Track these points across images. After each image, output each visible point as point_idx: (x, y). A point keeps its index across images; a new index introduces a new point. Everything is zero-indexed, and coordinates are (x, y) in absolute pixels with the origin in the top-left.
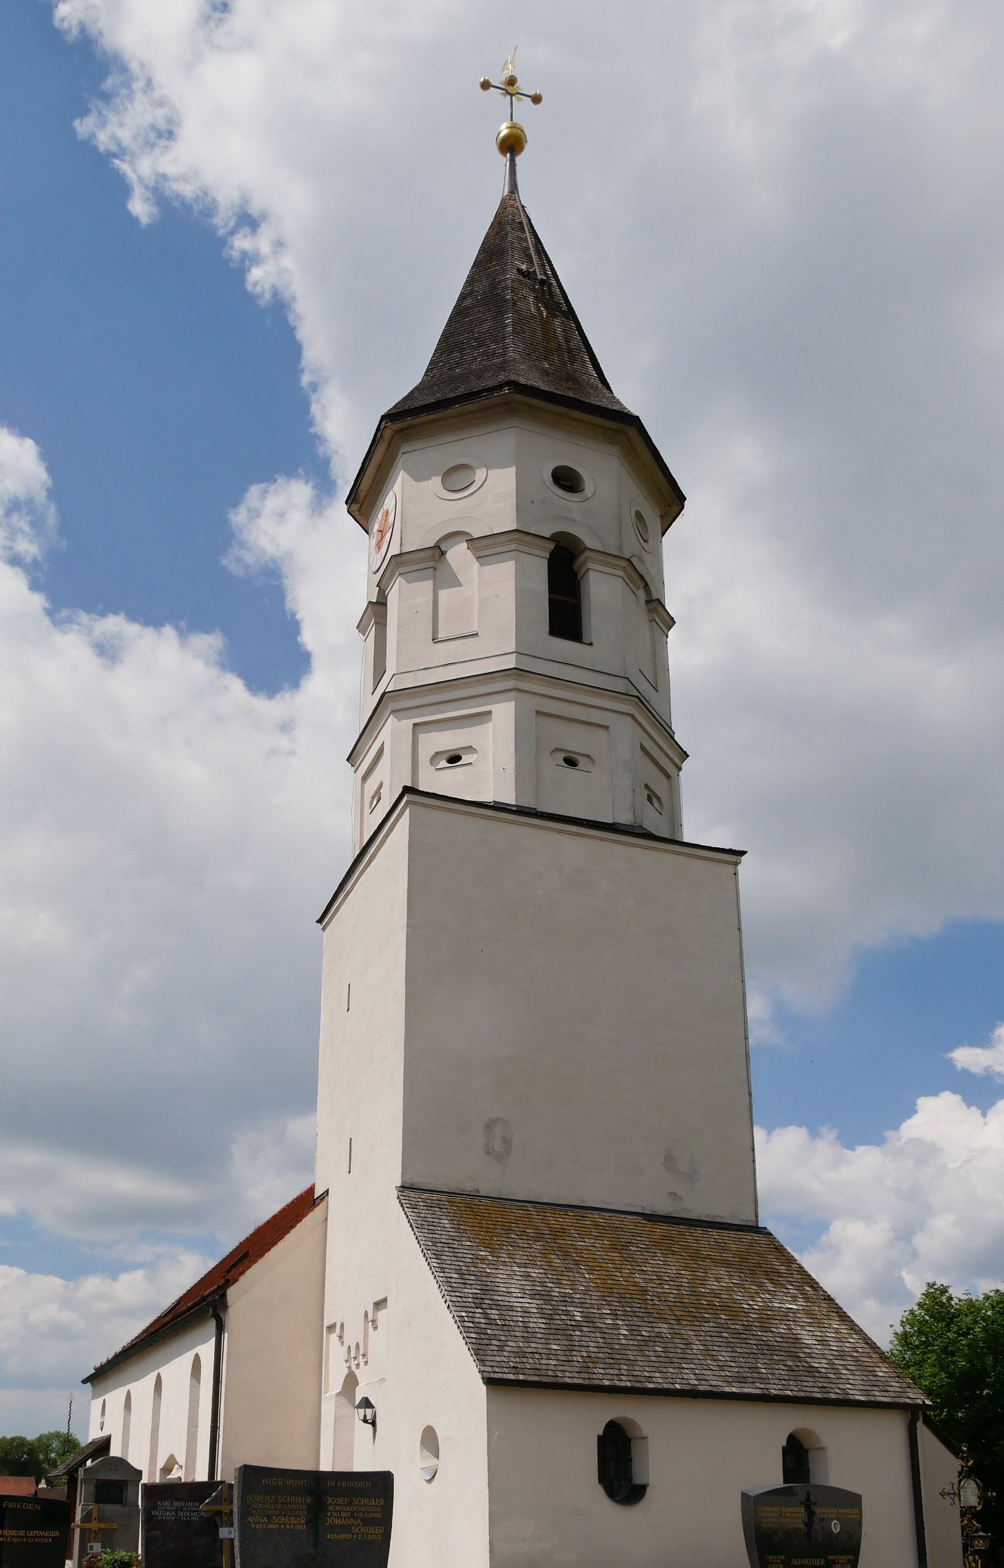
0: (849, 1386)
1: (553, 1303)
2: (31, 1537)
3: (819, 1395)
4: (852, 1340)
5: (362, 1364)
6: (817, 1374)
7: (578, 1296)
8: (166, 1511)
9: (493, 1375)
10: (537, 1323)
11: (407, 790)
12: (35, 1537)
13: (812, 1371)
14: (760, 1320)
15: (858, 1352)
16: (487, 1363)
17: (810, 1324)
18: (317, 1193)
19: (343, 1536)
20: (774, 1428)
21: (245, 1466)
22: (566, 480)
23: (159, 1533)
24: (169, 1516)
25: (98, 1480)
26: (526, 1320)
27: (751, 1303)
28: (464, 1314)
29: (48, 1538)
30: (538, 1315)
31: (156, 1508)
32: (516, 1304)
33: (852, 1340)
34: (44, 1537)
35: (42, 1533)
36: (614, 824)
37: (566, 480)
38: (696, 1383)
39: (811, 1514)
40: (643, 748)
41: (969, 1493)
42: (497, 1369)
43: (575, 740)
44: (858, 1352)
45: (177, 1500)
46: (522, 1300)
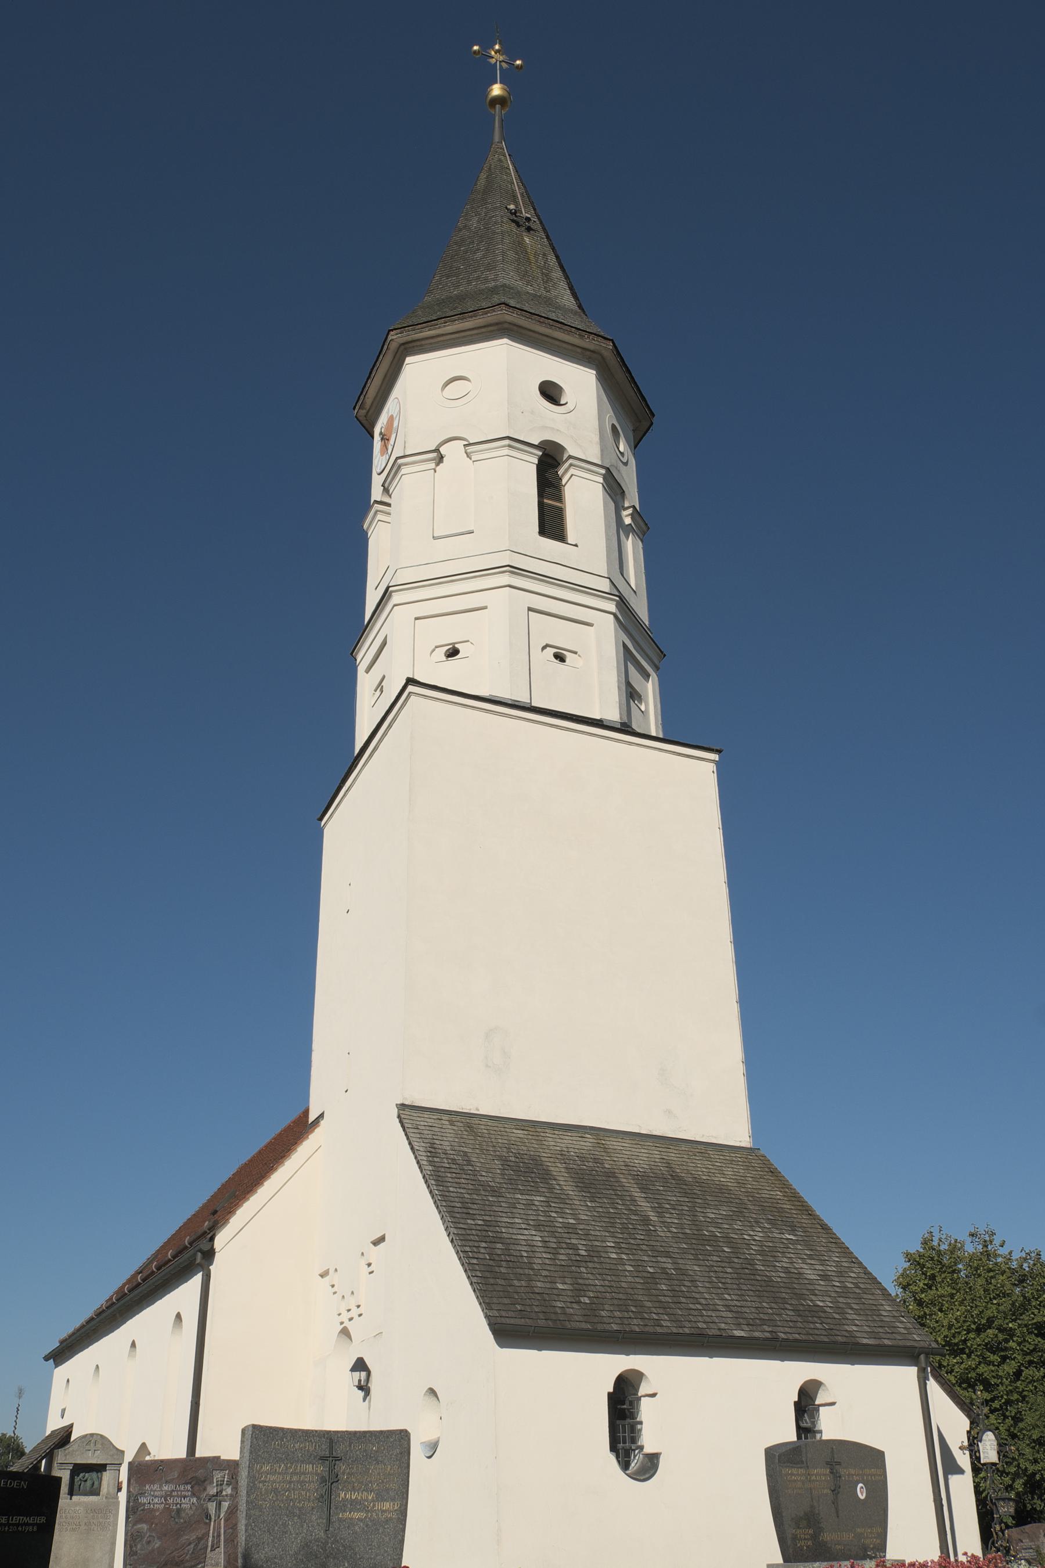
0: (855, 1328)
1: (557, 1235)
2: (13, 1525)
3: (826, 1339)
4: (853, 1275)
5: (356, 1317)
6: (822, 1315)
7: (581, 1227)
8: (154, 1497)
9: (499, 1320)
10: (542, 1257)
11: (410, 681)
12: (18, 1525)
13: (816, 1311)
14: (761, 1252)
15: (860, 1288)
16: (493, 1306)
17: (810, 1257)
18: (312, 1118)
19: (356, 1515)
20: (789, 1375)
21: (254, 1426)
22: (550, 392)
23: (144, 1527)
24: (157, 1503)
25: (75, 1465)
26: (531, 1254)
27: (752, 1233)
28: (468, 1249)
29: (33, 1525)
30: (542, 1250)
31: (142, 1494)
32: (519, 1237)
33: (853, 1275)
34: (27, 1524)
35: (26, 1520)
36: (601, 721)
37: (550, 392)
38: (705, 1326)
39: (835, 1475)
40: (625, 646)
41: (988, 1447)
42: (504, 1314)
43: (563, 635)
44: (860, 1288)
45: (166, 1482)
46: (526, 1232)
